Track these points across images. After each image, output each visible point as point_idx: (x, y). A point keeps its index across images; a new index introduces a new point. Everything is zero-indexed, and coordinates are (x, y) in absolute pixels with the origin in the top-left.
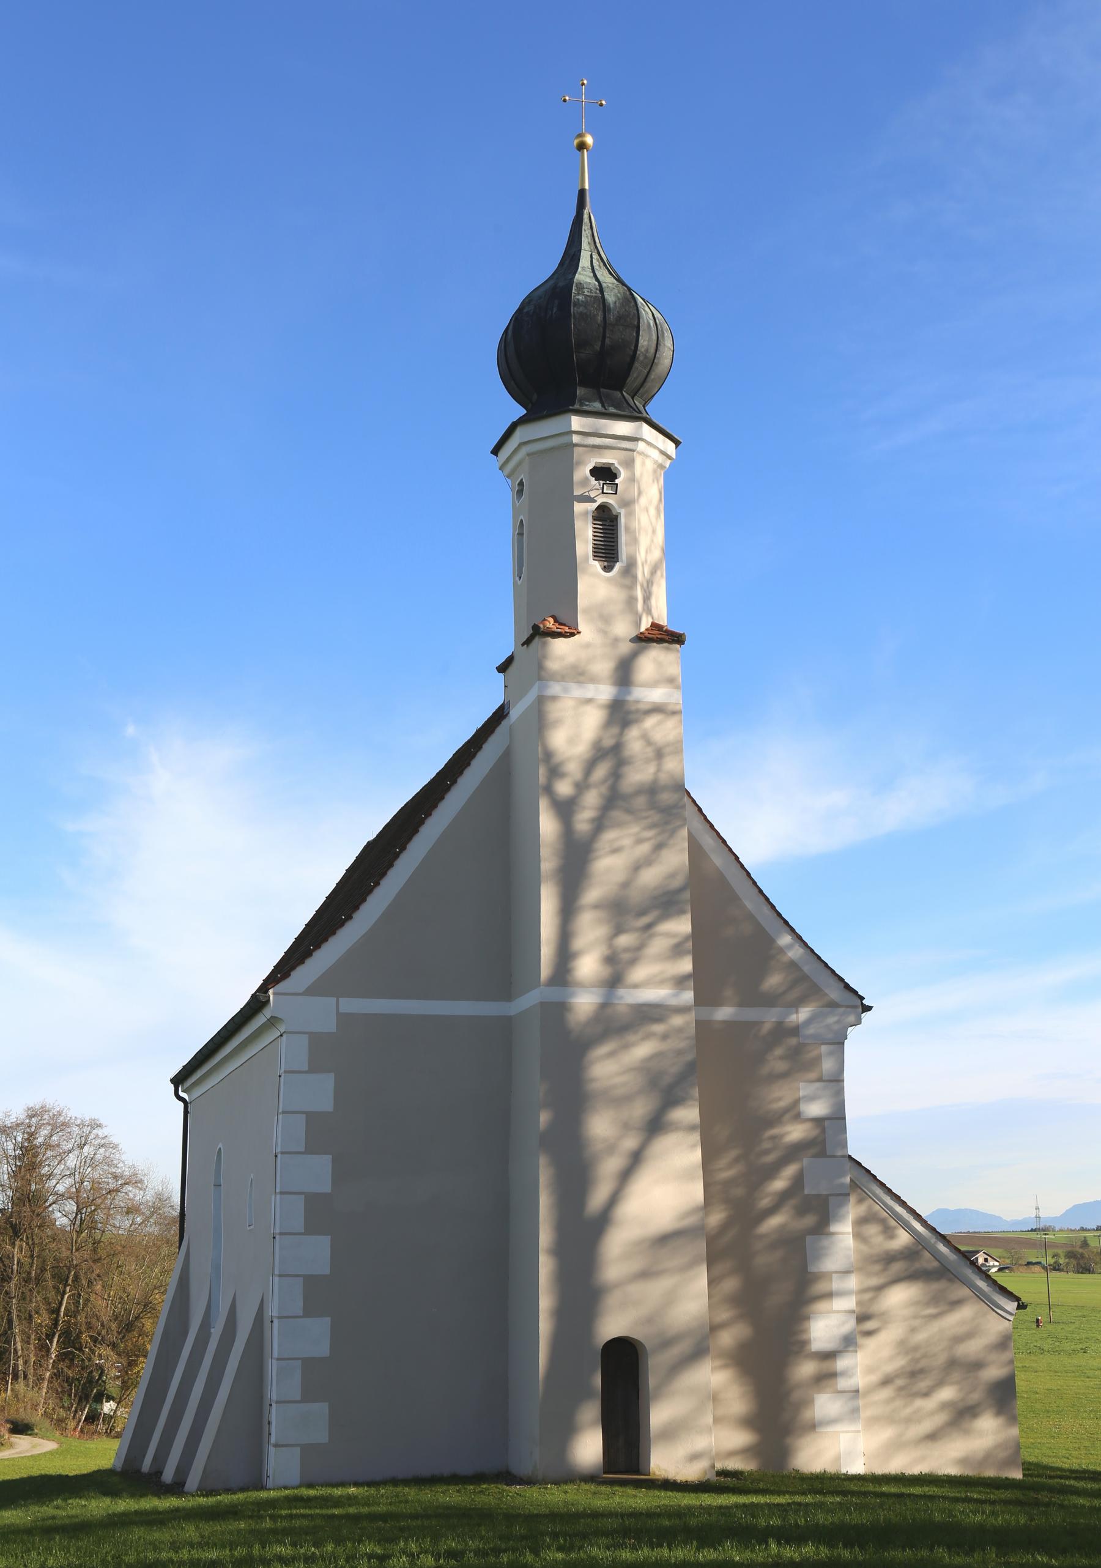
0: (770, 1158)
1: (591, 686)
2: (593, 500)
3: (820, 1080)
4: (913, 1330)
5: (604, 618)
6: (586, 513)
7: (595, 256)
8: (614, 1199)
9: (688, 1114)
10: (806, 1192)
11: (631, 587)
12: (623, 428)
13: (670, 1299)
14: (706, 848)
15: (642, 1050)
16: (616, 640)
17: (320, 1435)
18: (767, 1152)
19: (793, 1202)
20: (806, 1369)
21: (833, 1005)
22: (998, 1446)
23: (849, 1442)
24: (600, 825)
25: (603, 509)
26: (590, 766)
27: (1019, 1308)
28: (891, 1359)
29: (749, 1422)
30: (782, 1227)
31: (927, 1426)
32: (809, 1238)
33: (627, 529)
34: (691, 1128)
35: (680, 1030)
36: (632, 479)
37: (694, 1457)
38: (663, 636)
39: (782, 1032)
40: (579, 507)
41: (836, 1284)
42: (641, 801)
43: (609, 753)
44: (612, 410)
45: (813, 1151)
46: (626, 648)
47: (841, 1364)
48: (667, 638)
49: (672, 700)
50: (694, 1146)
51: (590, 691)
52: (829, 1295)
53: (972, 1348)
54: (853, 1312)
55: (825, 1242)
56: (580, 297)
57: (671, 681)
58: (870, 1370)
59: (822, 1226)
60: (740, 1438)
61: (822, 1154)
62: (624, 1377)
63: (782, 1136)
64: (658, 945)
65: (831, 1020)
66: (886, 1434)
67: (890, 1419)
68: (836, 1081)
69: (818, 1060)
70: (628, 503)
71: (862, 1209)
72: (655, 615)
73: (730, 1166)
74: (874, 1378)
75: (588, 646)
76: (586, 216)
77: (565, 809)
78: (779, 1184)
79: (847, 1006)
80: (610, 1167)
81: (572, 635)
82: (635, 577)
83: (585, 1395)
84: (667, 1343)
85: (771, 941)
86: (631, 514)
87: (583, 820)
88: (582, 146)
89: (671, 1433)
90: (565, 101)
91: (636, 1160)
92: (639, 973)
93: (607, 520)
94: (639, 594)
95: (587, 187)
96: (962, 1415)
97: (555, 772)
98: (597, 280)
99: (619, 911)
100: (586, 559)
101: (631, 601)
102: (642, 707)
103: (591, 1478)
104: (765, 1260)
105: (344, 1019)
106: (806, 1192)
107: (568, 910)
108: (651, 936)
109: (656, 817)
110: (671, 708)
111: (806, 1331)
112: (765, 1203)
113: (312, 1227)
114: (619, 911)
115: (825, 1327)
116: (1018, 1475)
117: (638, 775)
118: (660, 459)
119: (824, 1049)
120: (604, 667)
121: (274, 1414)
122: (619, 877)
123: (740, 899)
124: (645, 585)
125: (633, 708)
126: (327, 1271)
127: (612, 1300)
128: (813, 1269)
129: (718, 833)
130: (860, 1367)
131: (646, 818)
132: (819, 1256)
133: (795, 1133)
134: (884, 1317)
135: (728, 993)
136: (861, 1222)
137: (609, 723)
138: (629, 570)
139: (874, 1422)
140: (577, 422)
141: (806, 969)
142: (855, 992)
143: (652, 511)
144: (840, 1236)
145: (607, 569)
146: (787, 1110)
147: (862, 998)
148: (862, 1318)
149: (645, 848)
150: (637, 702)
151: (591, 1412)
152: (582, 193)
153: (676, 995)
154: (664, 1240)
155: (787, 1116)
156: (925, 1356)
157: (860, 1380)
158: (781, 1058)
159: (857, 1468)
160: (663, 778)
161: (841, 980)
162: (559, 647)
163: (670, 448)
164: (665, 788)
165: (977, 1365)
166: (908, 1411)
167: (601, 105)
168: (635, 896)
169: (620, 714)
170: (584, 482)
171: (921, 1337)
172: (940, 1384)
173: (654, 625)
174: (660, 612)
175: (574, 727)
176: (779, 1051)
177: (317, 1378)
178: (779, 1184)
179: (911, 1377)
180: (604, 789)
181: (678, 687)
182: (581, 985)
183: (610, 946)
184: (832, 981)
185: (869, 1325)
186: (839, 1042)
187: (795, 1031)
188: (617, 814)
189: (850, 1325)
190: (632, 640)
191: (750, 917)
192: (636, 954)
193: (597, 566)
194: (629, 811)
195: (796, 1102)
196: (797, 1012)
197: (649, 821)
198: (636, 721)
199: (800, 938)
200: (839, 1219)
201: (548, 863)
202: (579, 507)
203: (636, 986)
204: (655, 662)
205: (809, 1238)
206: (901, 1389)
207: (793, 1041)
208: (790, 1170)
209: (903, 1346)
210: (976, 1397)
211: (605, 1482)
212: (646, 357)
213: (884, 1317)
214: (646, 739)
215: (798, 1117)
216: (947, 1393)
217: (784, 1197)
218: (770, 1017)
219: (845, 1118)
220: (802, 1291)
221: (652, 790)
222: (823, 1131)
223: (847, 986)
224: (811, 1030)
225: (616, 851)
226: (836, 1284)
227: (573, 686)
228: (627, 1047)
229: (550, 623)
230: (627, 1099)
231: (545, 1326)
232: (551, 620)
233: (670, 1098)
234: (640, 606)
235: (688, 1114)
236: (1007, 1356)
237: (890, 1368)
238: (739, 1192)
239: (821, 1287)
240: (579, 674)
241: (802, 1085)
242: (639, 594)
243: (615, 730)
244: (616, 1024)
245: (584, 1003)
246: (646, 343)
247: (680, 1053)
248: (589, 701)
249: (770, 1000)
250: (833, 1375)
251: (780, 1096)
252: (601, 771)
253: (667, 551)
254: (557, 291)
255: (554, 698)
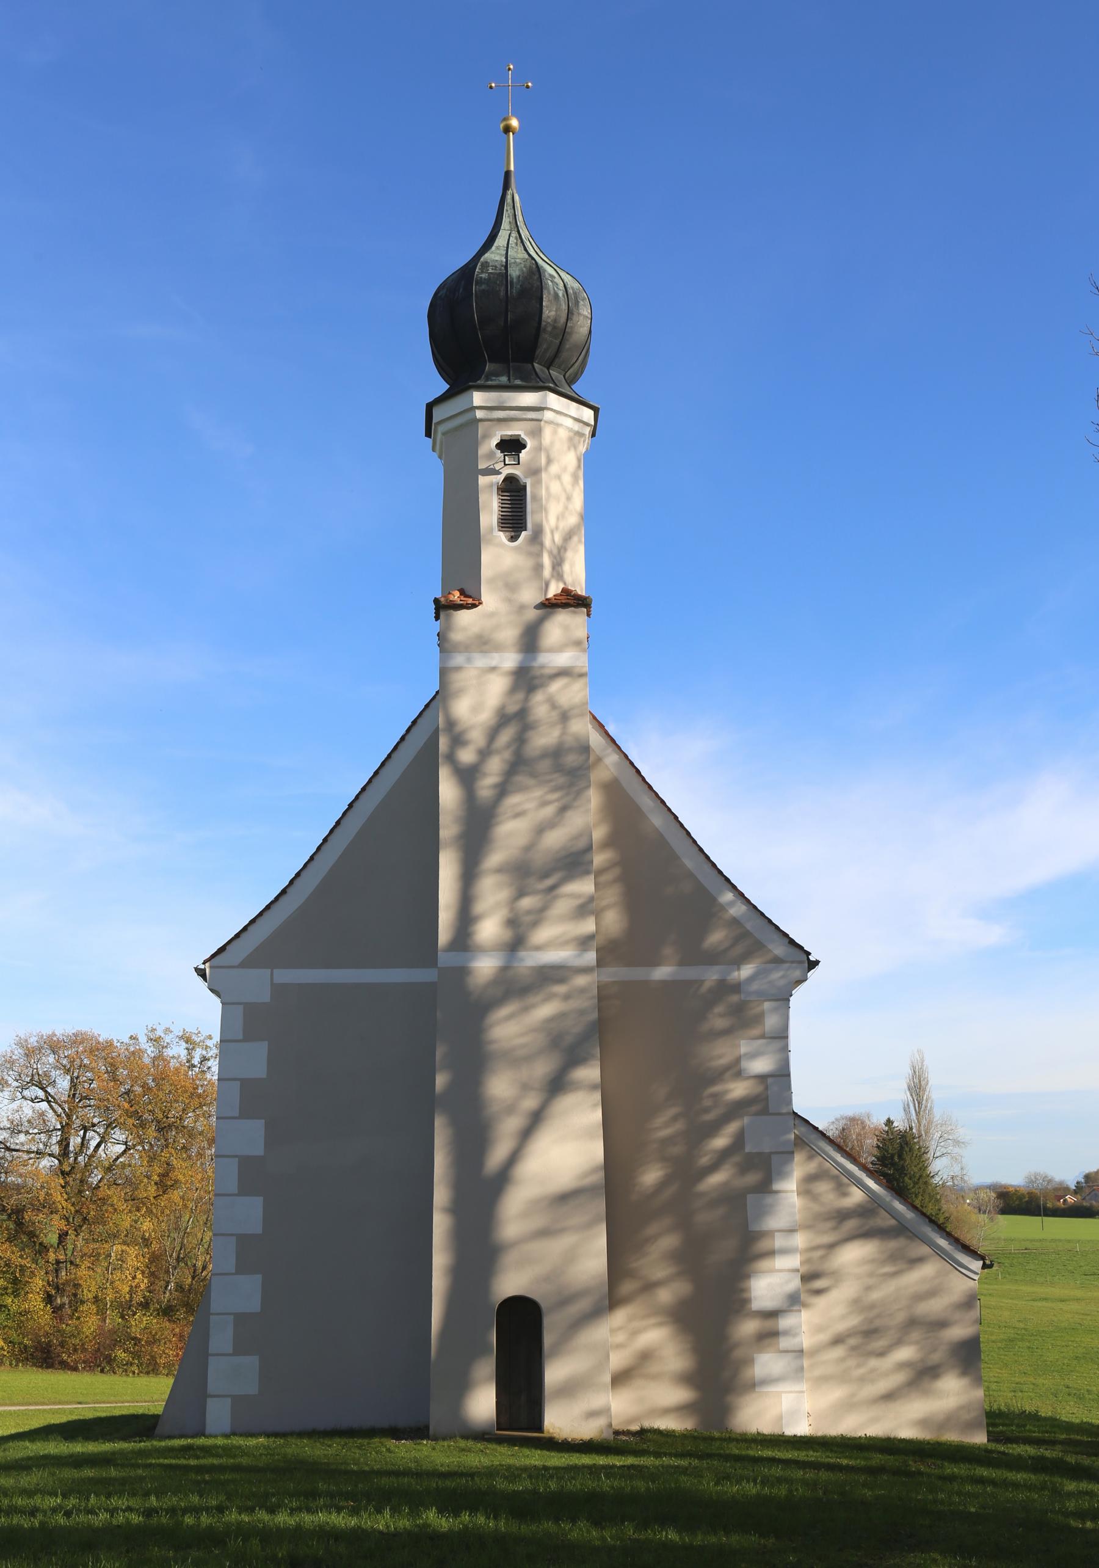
0: (709, 1117)
1: (496, 655)
2: (498, 473)
3: (763, 1036)
4: (868, 1288)
5: (510, 586)
6: (491, 485)
7: (514, 234)
8: (514, 1158)
9: (590, 1073)
10: (747, 1149)
11: (540, 555)
12: (528, 398)
13: (570, 1257)
14: (644, 809)
15: (545, 1011)
16: (522, 608)
17: (251, 1387)
18: (706, 1110)
19: (736, 1159)
20: (748, 1327)
21: (777, 961)
22: (961, 1408)
23: (793, 1402)
24: (503, 790)
25: (510, 480)
26: (493, 733)
27: (984, 1266)
28: (843, 1317)
29: (687, 1379)
30: (725, 1184)
31: (883, 1386)
32: (750, 1198)
33: (535, 498)
34: (593, 1087)
35: (582, 991)
36: (539, 448)
37: (592, 1414)
38: (571, 601)
39: (726, 988)
40: (483, 480)
41: (779, 1242)
42: (545, 765)
43: (514, 719)
44: (518, 382)
45: (754, 1109)
46: (532, 614)
47: (784, 1323)
48: (572, 602)
49: (579, 664)
50: (595, 1105)
51: (494, 659)
52: (771, 1253)
53: (935, 1307)
54: (798, 1271)
55: (769, 1199)
56: (483, 276)
57: (578, 643)
58: (819, 1329)
59: (765, 1187)
60: (679, 1395)
61: (765, 1112)
62: (521, 1336)
63: (727, 1092)
64: (562, 906)
65: (776, 975)
66: (836, 1394)
67: (842, 1378)
68: (781, 1036)
69: (759, 1019)
70: (535, 472)
71: (812, 1167)
72: (568, 578)
73: (667, 1125)
74: (824, 1337)
75: (492, 615)
76: (509, 197)
77: (467, 777)
78: (720, 1142)
79: (792, 962)
80: (508, 1128)
81: (474, 606)
82: (542, 544)
83: (484, 1351)
84: (565, 1300)
85: (713, 900)
86: (539, 482)
87: (486, 785)
88: (507, 129)
89: (570, 1389)
90: (491, 87)
91: (536, 1120)
92: (543, 934)
93: (514, 494)
94: (546, 560)
95: (512, 168)
96: (923, 1375)
97: (458, 740)
98: (507, 258)
99: (523, 873)
100: (491, 530)
101: (538, 568)
102: (547, 671)
103: (482, 1436)
104: (705, 1218)
105: (278, 990)
106: (747, 1149)
107: (469, 876)
108: (556, 897)
109: (561, 780)
110: (577, 671)
111: (747, 1290)
112: (704, 1161)
113: (245, 1189)
114: (523, 873)
115: (768, 1285)
116: (980, 1438)
117: (544, 738)
118: (576, 427)
119: (767, 1005)
120: (510, 634)
121: (213, 1363)
122: (521, 841)
123: (678, 858)
124: (555, 551)
125: (538, 673)
126: (259, 1230)
127: (509, 1259)
128: (754, 1227)
129: (657, 794)
130: (806, 1326)
131: (551, 781)
132: (763, 1211)
133: (738, 1090)
134: (836, 1276)
135: (668, 951)
136: (810, 1179)
137: (513, 689)
138: (537, 536)
139: (822, 1381)
140: (478, 398)
141: (749, 926)
142: (801, 948)
143: (567, 478)
144: (783, 1195)
145: (513, 539)
146: (727, 1068)
147: (808, 954)
148: (807, 1278)
149: (549, 811)
150: (542, 667)
151: (486, 1369)
152: (507, 174)
153: (579, 956)
154: (564, 1198)
155: (728, 1075)
156: (879, 1316)
157: (806, 1341)
158: (721, 1015)
159: (801, 1428)
160: (569, 741)
161: (786, 935)
162: (464, 618)
163: (588, 415)
164: (570, 750)
165: (942, 1324)
166: (861, 1371)
167: (528, 87)
168: (539, 858)
169: (526, 680)
170: (490, 456)
171: (875, 1296)
172: (899, 1343)
173: (566, 592)
174: (576, 574)
175: (479, 699)
176: (719, 1009)
177: (249, 1333)
178: (720, 1142)
179: (866, 1336)
180: (507, 755)
181: (584, 651)
182: (481, 950)
183: (512, 910)
184: (776, 936)
185: (819, 1284)
186: (784, 999)
187: (737, 988)
188: (520, 779)
189: (795, 1283)
190: (537, 607)
191: (690, 875)
192: (538, 916)
193: (502, 537)
194: (533, 775)
195: (738, 1060)
196: (739, 969)
197: (553, 784)
198: (542, 685)
199: (742, 895)
200: (783, 1175)
201: (448, 829)
202: (483, 480)
203: (538, 948)
204: (563, 627)
205: (750, 1198)
206: (854, 1348)
207: (734, 998)
208: (732, 1128)
209: (857, 1304)
210: (936, 1357)
211: (500, 1441)
212: (554, 328)
213: (836, 1276)
214: (553, 705)
215: (739, 1074)
216: (905, 1353)
217: (724, 1155)
218: (711, 975)
219: (789, 1075)
220: (748, 1250)
221: (556, 753)
222: (766, 1088)
223: (792, 942)
224: (755, 987)
225: (518, 815)
226: (779, 1242)
227: (476, 655)
228: (526, 1009)
229: (456, 596)
230: (528, 1059)
231: (439, 1283)
232: (457, 594)
233: (573, 1057)
234: (547, 572)
235: (590, 1073)
236: (975, 1314)
237: (841, 1327)
238: (677, 1150)
239: (764, 1245)
240: (483, 643)
241: (742, 1042)
242: (546, 560)
243: (520, 696)
244: (515, 987)
245: (485, 966)
246: (553, 313)
247: (582, 1012)
248: (493, 669)
249: (712, 958)
250: (774, 1334)
251: (720, 1053)
252: (506, 736)
253: (587, 515)
254: (466, 273)
255: (458, 669)
